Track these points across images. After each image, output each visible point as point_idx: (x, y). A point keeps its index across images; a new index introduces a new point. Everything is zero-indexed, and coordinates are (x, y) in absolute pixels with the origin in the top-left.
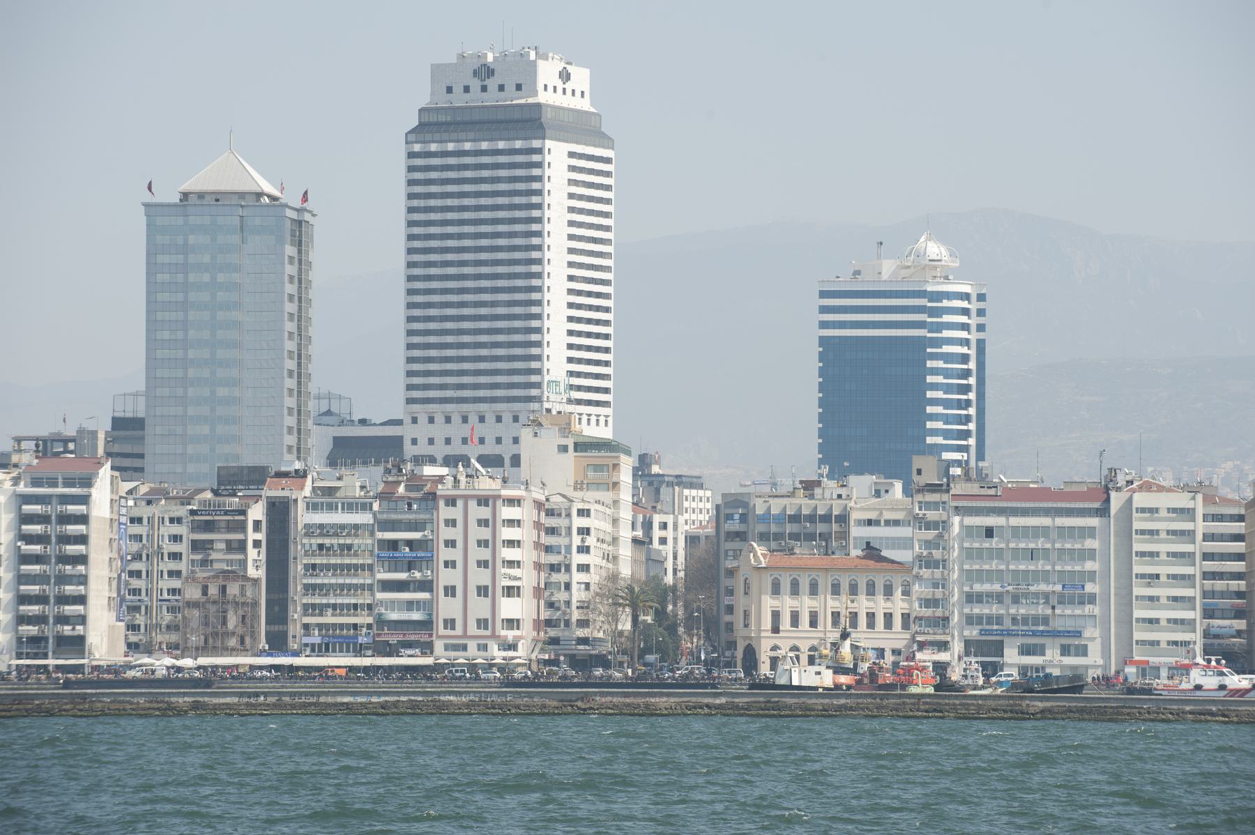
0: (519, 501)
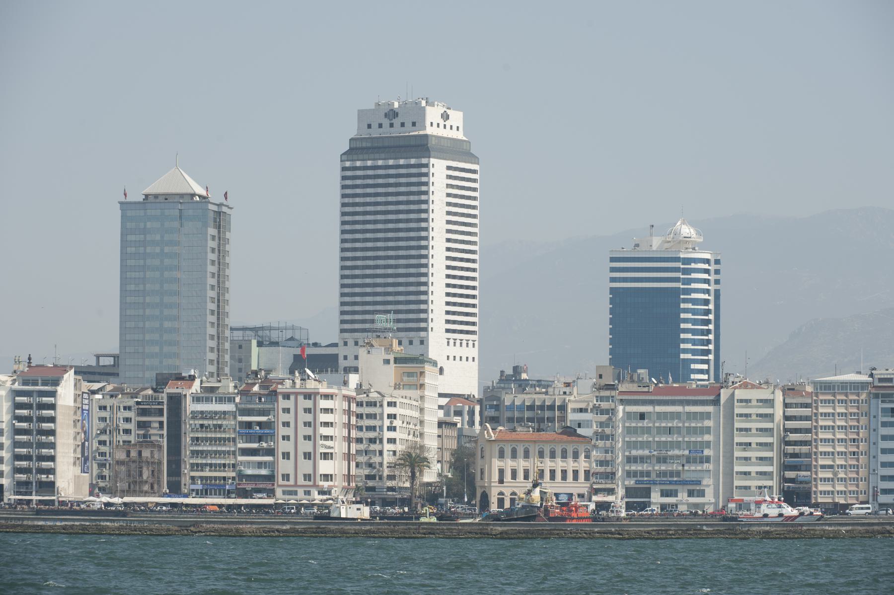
0: (332, 396)
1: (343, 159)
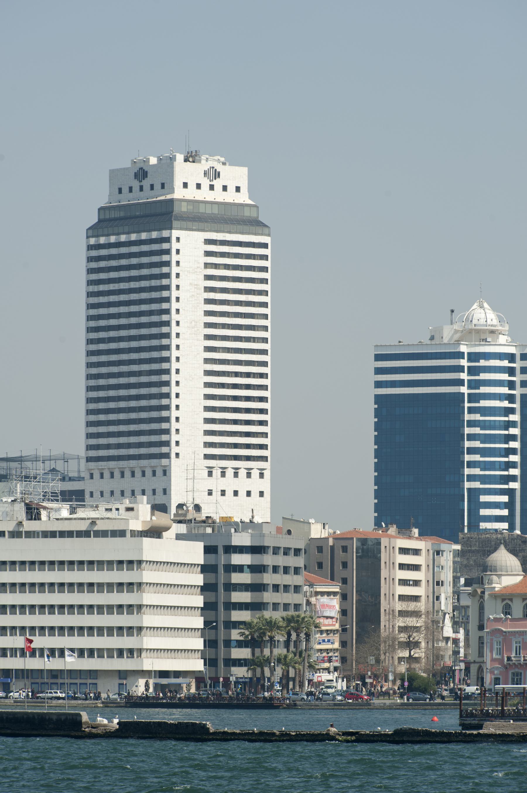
1: (89, 235)
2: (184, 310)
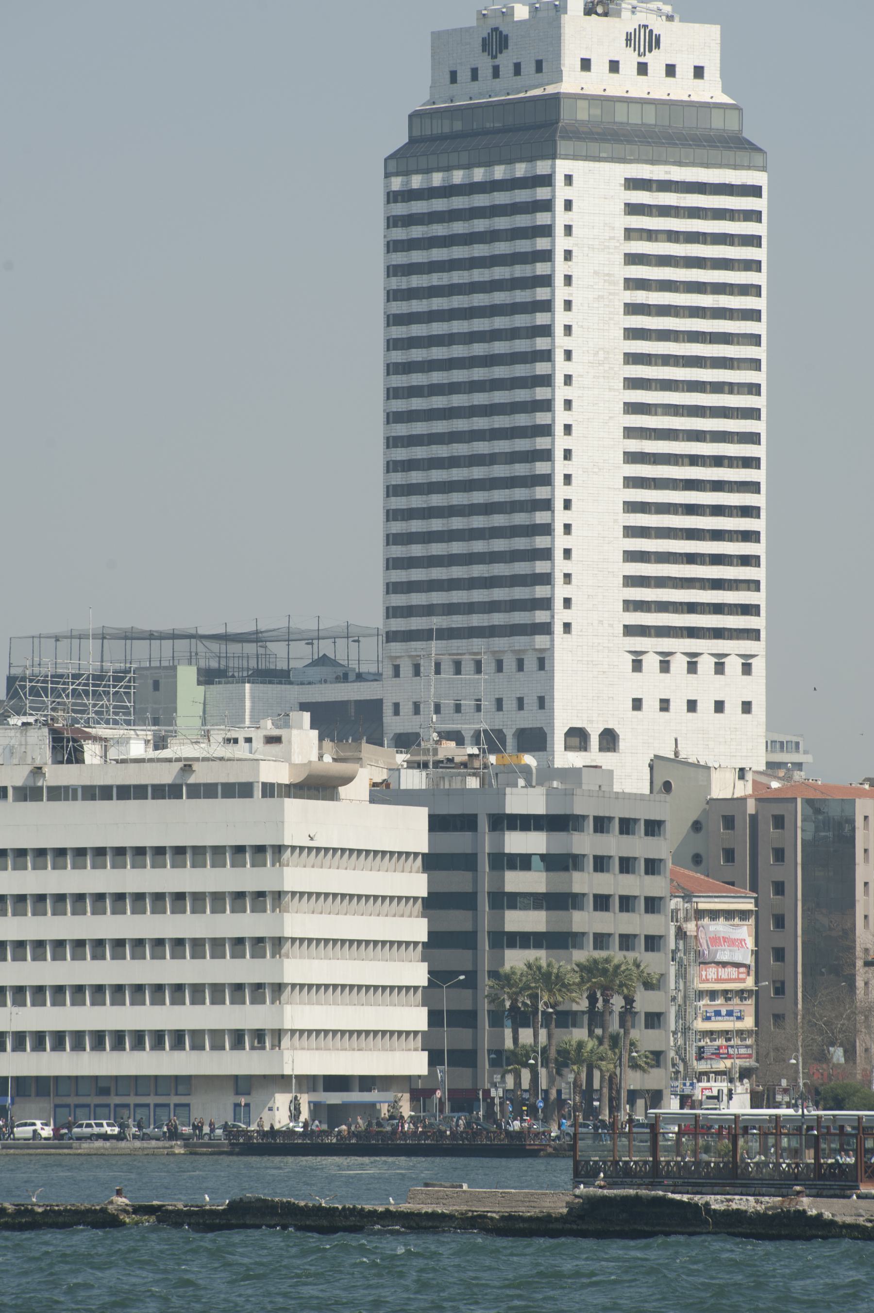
2: (582, 327)
